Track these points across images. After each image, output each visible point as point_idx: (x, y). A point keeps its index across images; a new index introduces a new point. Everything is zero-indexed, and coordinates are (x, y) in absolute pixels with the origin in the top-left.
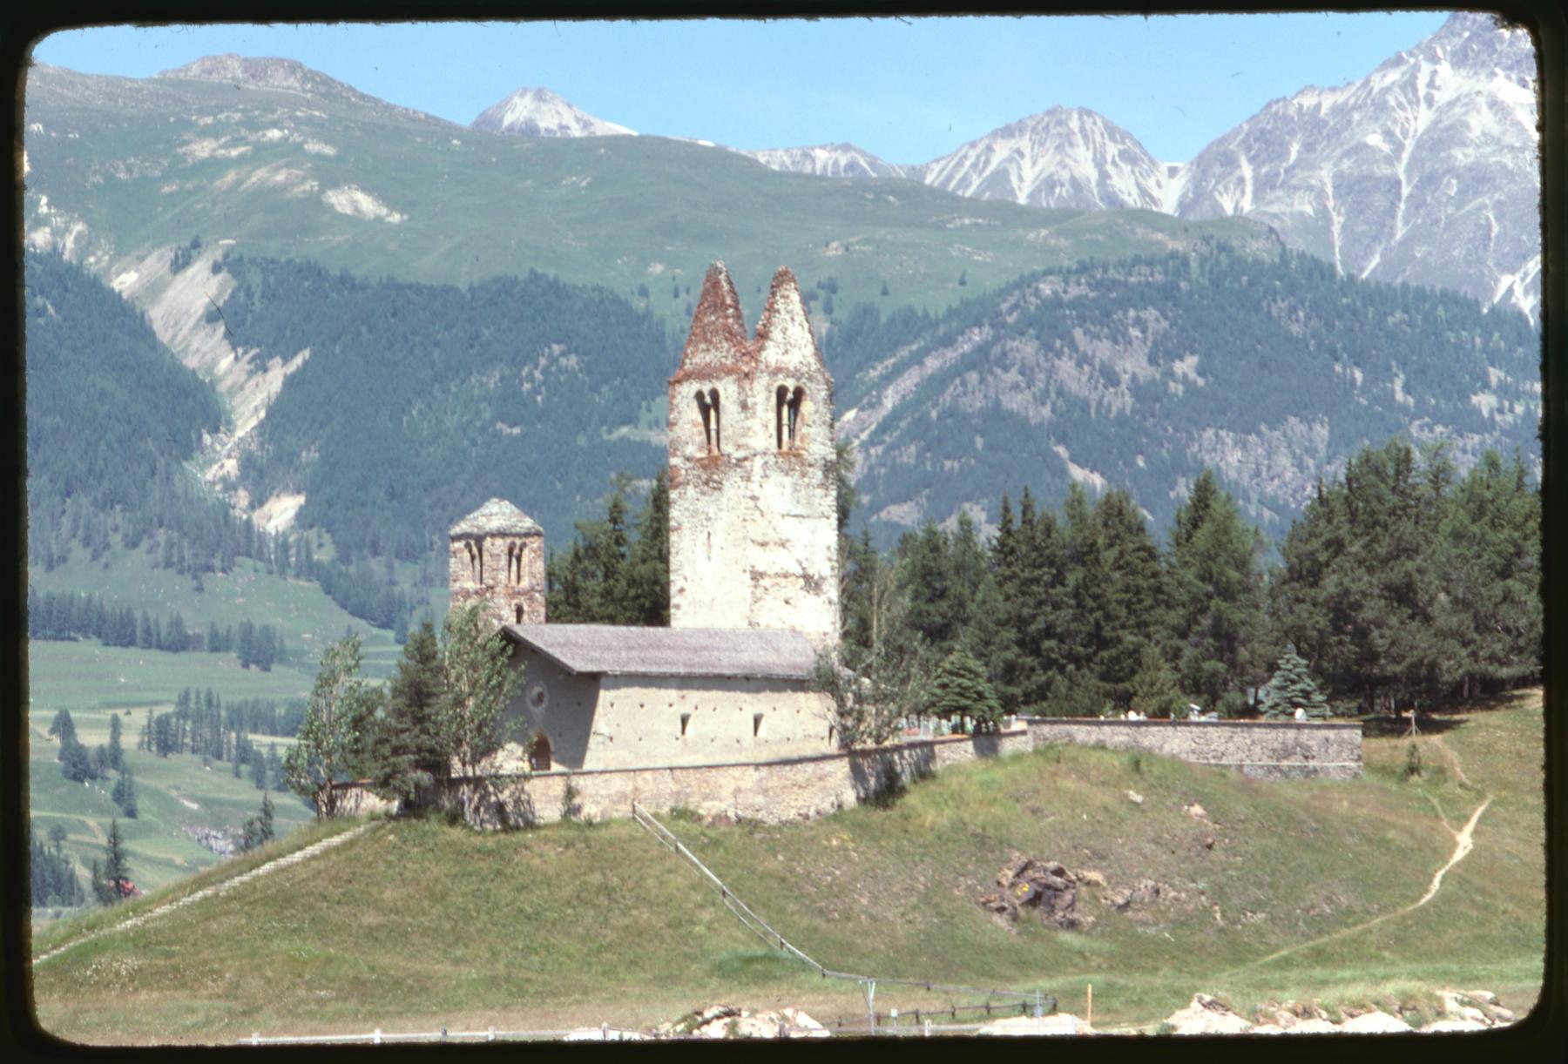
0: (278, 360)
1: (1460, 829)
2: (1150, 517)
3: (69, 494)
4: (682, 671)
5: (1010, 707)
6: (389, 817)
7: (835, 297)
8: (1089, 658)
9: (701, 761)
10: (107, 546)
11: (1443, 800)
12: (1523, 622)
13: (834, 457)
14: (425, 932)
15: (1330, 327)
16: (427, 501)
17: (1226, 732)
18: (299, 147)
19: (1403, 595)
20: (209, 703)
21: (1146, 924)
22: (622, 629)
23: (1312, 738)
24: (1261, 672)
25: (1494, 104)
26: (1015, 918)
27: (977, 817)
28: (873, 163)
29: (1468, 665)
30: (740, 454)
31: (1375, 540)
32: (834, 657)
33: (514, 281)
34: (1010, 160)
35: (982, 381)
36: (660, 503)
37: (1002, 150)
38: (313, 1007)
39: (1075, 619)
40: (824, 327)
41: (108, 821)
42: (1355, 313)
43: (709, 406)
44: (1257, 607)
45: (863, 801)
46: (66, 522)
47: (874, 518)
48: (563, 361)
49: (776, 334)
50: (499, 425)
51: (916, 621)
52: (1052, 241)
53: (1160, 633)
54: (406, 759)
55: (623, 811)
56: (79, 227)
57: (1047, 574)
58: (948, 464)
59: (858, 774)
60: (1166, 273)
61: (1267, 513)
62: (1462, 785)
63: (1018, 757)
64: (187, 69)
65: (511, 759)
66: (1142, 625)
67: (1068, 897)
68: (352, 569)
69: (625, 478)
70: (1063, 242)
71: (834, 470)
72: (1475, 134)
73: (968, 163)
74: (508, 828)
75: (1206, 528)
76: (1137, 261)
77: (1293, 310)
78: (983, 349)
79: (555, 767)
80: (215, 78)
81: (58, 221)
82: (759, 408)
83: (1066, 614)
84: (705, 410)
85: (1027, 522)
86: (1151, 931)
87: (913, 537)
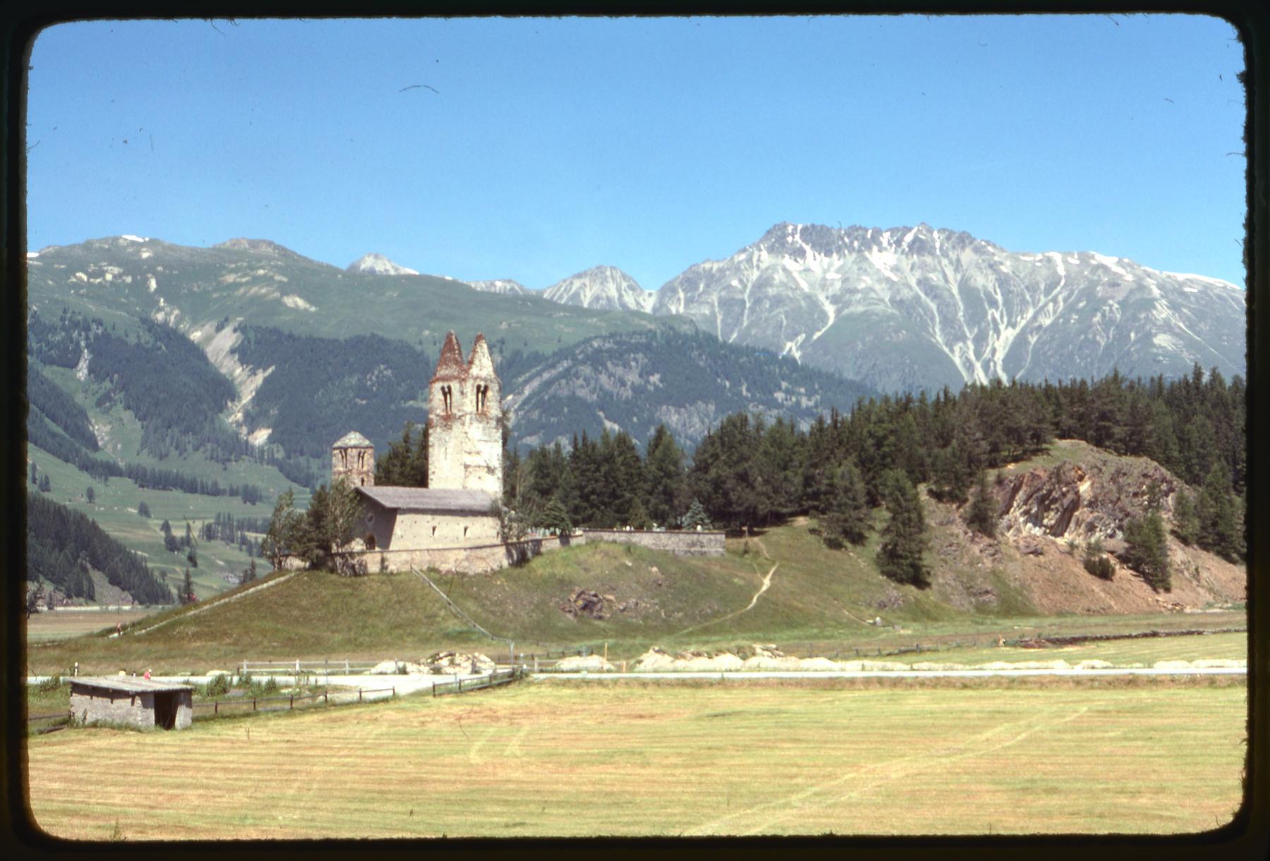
0: (261, 370)
1: (765, 577)
2: (638, 443)
3: (169, 427)
4: (434, 507)
5: (576, 524)
6: (305, 569)
7: (504, 347)
8: (610, 503)
9: (440, 546)
10: (185, 450)
11: (759, 565)
12: (793, 489)
13: (500, 415)
14: (319, 619)
15: (715, 362)
16: (324, 432)
17: (668, 535)
18: (272, 278)
19: (743, 478)
20: (229, 519)
21: (631, 617)
22: (407, 489)
23: (705, 539)
24: (684, 510)
25: (784, 269)
26: (576, 615)
27: (560, 571)
28: (521, 288)
29: (769, 507)
30: (460, 414)
31: (732, 454)
32: (500, 503)
33: (364, 338)
34: (581, 288)
35: (567, 383)
36: (426, 435)
37: (577, 284)
38: (271, 650)
39: (605, 487)
40: (499, 359)
41: (185, 569)
42: (726, 357)
43: (447, 393)
44: (682, 482)
45: (511, 565)
46: (168, 440)
47: (519, 443)
48: (385, 372)
49: (477, 362)
50: (357, 400)
51: (536, 487)
52: (598, 324)
53: (641, 493)
54: (313, 544)
55: (406, 568)
56: (176, 312)
57: (593, 467)
58: (552, 419)
59: (509, 554)
60: (647, 338)
61: (688, 442)
62: (766, 559)
63: (579, 546)
64: (224, 244)
65: (357, 545)
66: (633, 490)
67: (599, 606)
68: (292, 461)
69: (410, 424)
70: (604, 324)
71: (501, 421)
72: (776, 282)
73: (562, 289)
74: (356, 574)
75: (661, 448)
76: (635, 333)
77: (700, 355)
78: (568, 370)
79: (377, 549)
80: (236, 248)
81: (168, 309)
82: (469, 394)
83: (601, 484)
84: (445, 394)
85: (585, 444)
86: (634, 620)
87: (535, 451)
